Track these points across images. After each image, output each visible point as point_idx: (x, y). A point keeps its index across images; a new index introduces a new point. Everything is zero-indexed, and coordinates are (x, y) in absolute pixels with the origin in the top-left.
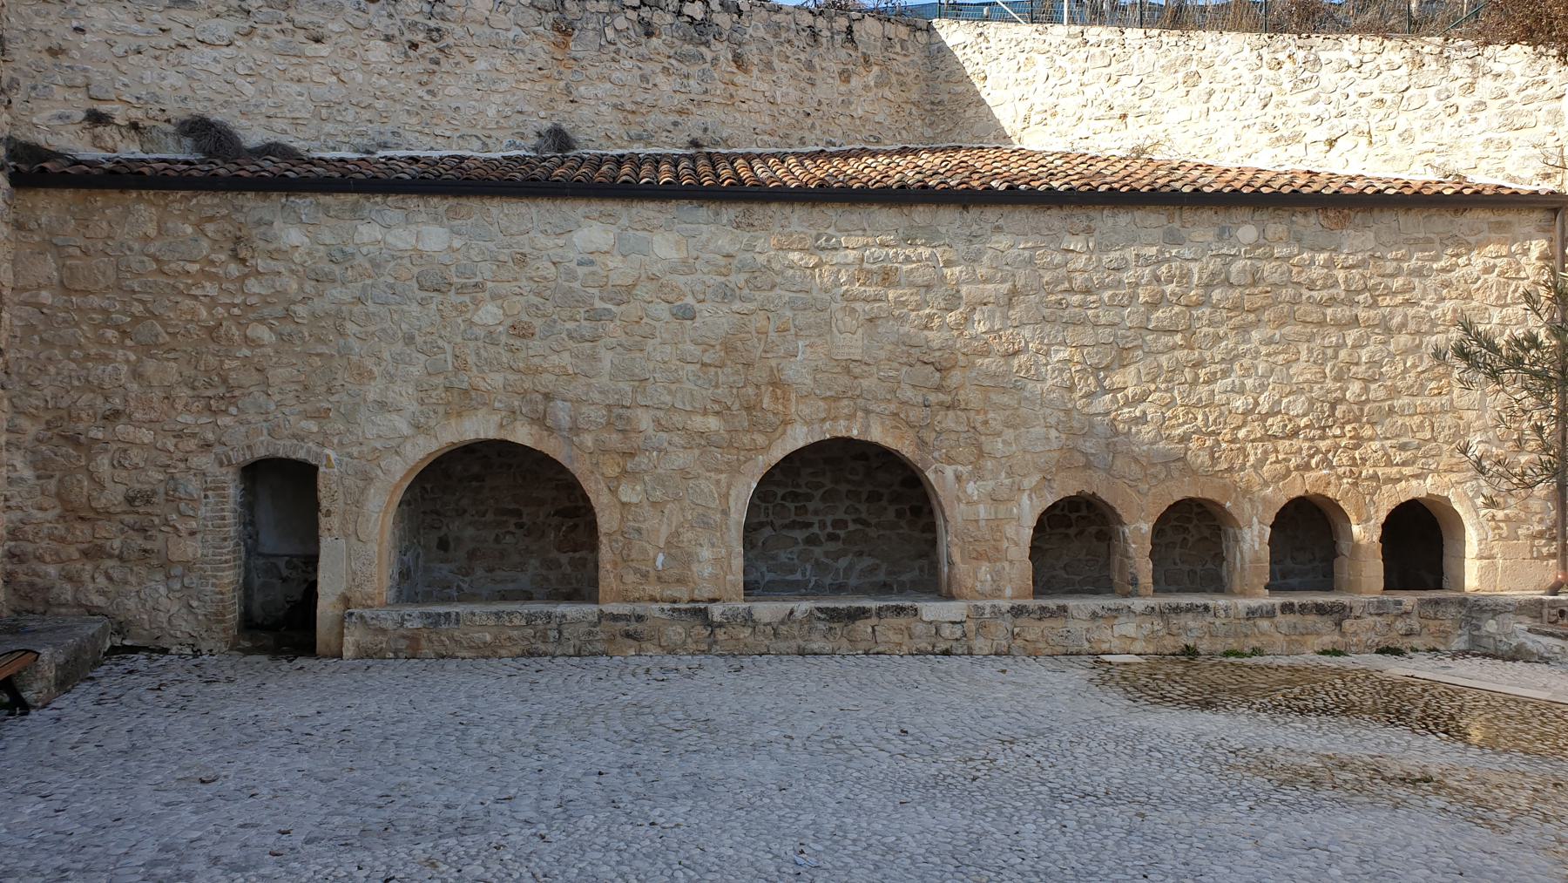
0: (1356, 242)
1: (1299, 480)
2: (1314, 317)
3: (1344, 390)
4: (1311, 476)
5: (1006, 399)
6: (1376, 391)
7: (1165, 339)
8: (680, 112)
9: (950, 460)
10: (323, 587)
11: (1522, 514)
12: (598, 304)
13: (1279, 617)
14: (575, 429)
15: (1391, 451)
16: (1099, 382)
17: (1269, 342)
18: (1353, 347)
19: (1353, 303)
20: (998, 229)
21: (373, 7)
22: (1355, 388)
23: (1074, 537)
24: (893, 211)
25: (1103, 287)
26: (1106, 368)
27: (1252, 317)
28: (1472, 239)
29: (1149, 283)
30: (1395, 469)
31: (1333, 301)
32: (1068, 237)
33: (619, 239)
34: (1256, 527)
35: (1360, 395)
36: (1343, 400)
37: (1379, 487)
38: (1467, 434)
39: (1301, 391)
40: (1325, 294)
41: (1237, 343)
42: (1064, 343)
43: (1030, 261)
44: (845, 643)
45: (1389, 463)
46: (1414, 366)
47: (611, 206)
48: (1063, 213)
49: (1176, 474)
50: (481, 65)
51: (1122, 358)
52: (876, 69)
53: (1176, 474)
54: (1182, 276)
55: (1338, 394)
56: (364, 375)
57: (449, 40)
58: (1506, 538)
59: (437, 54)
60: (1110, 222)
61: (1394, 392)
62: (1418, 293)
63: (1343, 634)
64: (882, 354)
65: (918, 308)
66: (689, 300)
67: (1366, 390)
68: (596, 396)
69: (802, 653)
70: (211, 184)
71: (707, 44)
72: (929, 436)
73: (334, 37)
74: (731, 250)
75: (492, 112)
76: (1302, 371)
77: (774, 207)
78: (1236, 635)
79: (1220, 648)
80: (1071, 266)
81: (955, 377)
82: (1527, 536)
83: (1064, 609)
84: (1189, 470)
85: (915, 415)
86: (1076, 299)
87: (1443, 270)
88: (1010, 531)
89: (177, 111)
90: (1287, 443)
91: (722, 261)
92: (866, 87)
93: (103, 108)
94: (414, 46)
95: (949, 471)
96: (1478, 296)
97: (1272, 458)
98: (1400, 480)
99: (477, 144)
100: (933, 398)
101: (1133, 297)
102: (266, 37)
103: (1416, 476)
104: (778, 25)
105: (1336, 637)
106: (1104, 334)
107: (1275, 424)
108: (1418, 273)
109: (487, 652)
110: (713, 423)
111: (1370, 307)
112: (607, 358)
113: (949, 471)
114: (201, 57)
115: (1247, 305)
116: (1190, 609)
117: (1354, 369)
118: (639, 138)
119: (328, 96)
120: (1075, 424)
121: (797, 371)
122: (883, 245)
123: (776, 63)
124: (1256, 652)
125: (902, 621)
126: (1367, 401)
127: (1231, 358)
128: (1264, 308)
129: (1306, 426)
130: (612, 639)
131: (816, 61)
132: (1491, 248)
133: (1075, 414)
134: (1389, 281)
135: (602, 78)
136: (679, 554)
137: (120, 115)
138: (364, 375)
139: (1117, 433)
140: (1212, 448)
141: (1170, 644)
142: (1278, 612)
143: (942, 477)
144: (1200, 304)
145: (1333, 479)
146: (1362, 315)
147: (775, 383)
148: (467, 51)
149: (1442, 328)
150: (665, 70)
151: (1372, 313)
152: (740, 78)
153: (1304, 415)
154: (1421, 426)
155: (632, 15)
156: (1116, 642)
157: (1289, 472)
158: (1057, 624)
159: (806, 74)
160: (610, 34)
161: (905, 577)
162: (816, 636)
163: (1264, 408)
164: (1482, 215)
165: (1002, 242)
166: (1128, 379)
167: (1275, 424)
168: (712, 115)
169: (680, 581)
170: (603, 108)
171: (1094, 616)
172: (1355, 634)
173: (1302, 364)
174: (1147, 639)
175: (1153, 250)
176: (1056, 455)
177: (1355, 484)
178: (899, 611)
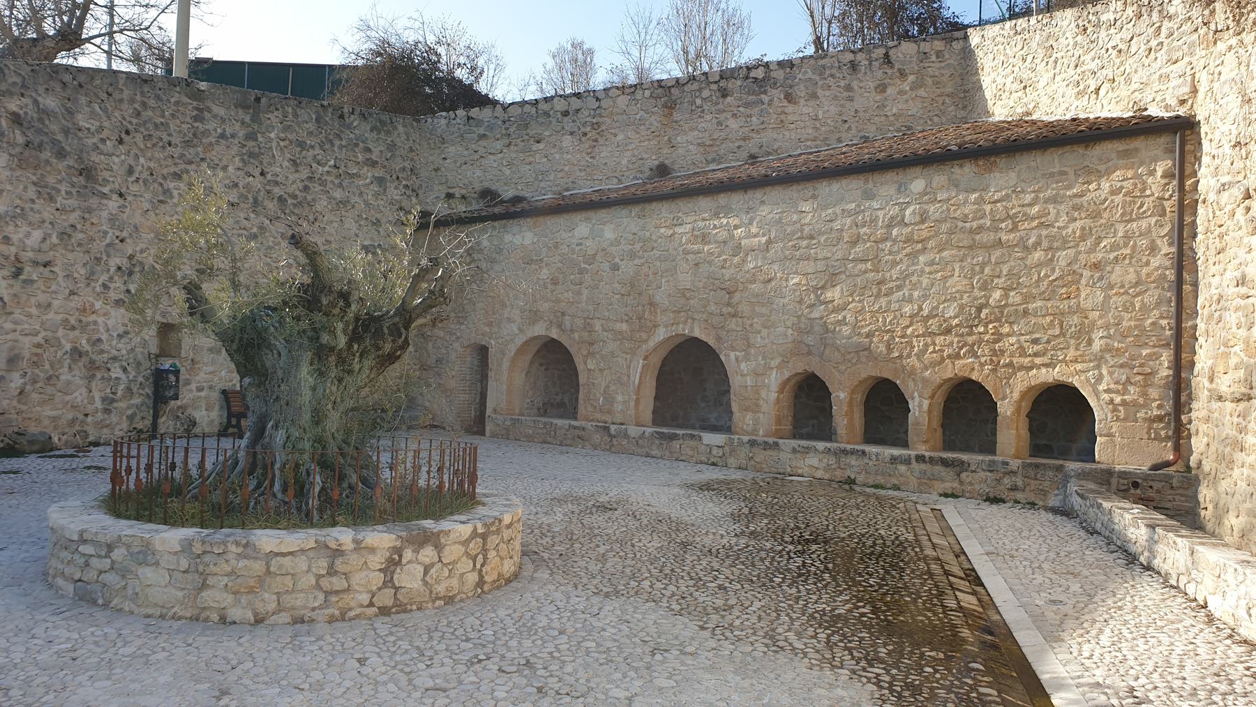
0: (1001, 182)
1: (950, 366)
2: (965, 243)
4: (959, 363)
5: (763, 310)
6: (1014, 297)
7: (862, 266)
8: (744, 139)
9: (733, 349)
10: (488, 404)
11: (1141, 401)
12: (583, 265)
13: (914, 464)
14: (572, 331)
16: (818, 297)
17: (932, 263)
18: (996, 263)
19: (997, 230)
20: (763, 202)
22: (997, 294)
23: (809, 402)
24: (709, 199)
25: (821, 233)
26: (823, 287)
27: (920, 246)
28: (1102, 168)
29: (850, 227)
30: (1028, 359)
31: (981, 229)
32: (802, 203)
33: (592, 230)
34: (917, 399)
35: (1000, 301)
36: (986, 305)
38: (1092, 331)
39: (955, 299)
40: (975, 224)
41: (908, 266)
42: (796, 273)
44: (667, 453)
45: (1023, 353)
46: (1047, 276)
47: (590, 214)
48: (800, 188)
50: (620, 137)
51: (832, 279)
52: (911, 78)
53: (864, 360)
54: (872, 221)
55: (983, 301)
56: (504, 305)
57: (604, 127)
58: (1125, 419)
60: (827, 189)
61: (1028, 298)
62: (1052, 217)
63: (961, 483)
64: (701, 285)
65: (719, 256)
66: (617, 260)
68: (580, 313)
69: (647, 456)
70: (494, 217)
71: (765, 92)
72: (723, 334)
74: (635, 231)
75: (624, 162)
76: (957, 282)
77: (654, 204)
78: (883, 474)
79: (871, 482)
80: (803, 222)
81: (737, 296)
82: (1145, 419)
83: (776, 444)
85: (715, 320)
86: (805, 243)
87: (1075, 196)
88: (763, 394)
89: (478, 187)
91: (631, 237)
92: (901, 93)
93: (451, 191)
94: (585, 134)
95: (732, 355)
96: (1106, 215)
98: (1031, 368)
99: (615, 180)
100: (725, 310)
101: (839, 239)
103: (1046, 365)
104: (824, 67)
105: (956, 485)
106: (821, 266)
107: (934, 324)
108: (1054, 200)
109: (530, 439)
110: (624, 326)
111: (1011, 231)
112: (585, 292)
113: (732, 355)
115: (916, 237)
116: (853, 452)
118: (714, 160)
120: (802, 326)
121: (661, 297)
122: (704, 220)
123: (820, 92)
124: (896, 488)
125: (693, 443)
126: (1006, 305)
127: (905, 276)
128: (929, 238)
129: (957, 325)
130: (573, 439)
131: (855, 84)
132: (1118, 173)
133: (803, 319)
134: (1027, 209)
135: (692, 129)
136: (610, 399)
137: (458, 192)
138: (504, 305)
139: (827, 331)
140: (888, 341)
141: (839, 474)
142: (913, 461)
143: (729, 358)
145: (976, 366)
146: (1004, 238)
147: (652, 304)
150: (734, 116)
151: (1012, 236)
152: (790, 109)
153: (955, 317)
154: (1051, 324)
155: (714, 87)
156: (806, 469)
157: (943, 360)
158: (773, 453)
159: (846, 94)
160: (698, 102)
161: (804, 431)
162: (654, 447)
163: (925, 313)
164: (1110, 146)
165: (764, 211)
166: (834, 294)
167: (934, 324)
168: (767, 137)
169: (609, 412)
170: (691, 147)
171: (794, 451)
172: (970, 483)
173: (956, 278)
174: (826, 470)
177: (994, 370)
178: (692, 436)
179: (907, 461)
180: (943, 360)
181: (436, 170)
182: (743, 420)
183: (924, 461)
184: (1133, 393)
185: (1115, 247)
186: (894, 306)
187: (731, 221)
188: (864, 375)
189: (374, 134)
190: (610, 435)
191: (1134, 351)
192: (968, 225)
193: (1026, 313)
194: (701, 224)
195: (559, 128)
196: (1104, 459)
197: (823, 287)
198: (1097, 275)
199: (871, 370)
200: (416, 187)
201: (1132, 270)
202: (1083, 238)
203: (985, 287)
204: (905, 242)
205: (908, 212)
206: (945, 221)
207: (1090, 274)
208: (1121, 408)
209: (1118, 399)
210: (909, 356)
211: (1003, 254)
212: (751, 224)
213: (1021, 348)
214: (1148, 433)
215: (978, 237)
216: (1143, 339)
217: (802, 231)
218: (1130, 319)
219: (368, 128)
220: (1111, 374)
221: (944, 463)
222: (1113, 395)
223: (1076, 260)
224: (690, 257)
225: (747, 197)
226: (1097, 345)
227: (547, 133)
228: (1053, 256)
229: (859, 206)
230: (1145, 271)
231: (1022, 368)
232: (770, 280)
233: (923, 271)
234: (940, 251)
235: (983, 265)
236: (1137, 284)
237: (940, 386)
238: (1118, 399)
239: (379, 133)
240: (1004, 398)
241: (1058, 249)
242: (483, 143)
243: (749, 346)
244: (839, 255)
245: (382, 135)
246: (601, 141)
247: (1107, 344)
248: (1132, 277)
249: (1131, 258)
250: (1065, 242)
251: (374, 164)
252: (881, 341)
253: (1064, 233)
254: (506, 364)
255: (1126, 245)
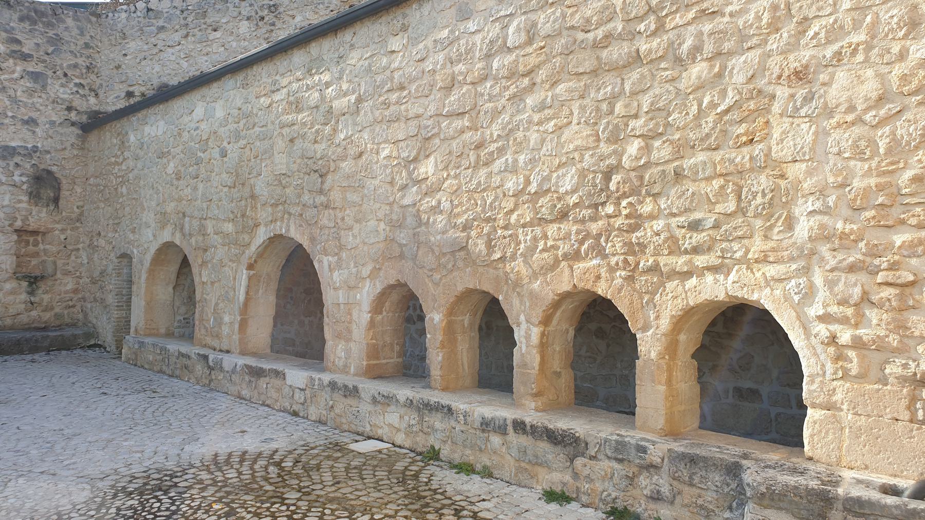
1: (567, 271)
2: (587, 66)
3: (619, 154)
4: (580, 266)
6: (661, 151)
7: (458, 123)
9: (325, 252)
11: (894, 340)
13: (512, 436)
15: (679, 233)
16: (410, 174)
17: (542, 107)
19: (633, 35)
21: (243, 3)
22: (633, 147)
25: (412, 80)
26: (415, 160)
27: (526, 81)
29: (444, 66)
35: (638, 159)
37: (663, 284)
40: (600, 33)
41: (512, 116)
43: (369, 70)
45: (674, 248)
46: (713, 105)
47: (204, 91)
49: (460, 264)
53: (460, 264)
55: (612, 161)
58: (861, 377)
59: (274, 20)
61: (681, 149)
63: (576, 476)
67: (648, 149)
73: (224, 25)
76: (576, 135)
78: (472, 447)
80: (392, 66)
82: (903, 380)
84: (471, 260)
86: (394, 97)
90: (555, 226)
93: (131, 89)
94: (262, 18)
97: (541, 245)
98: (688, 275)
102: (194, 36)
105: (568, 478)
111: (654, 34)
114: (169, 55)
117: (632, 123)
119: (219, 59)
120: (395, 217)
121: (261, 188)
125: (277, 382)
128: (538, 67)
129: (576, 205)
139: (420, 223)
140: (489, 234)
142: (510, 429)
144: (485, 78)
145: (603, 272)
146: (644, 48)
147: (253, 197)
148: (290, 13)
149: (755, 41)
153: (574, 191)
156: (386, 429)
157: (557, 262)
163: (533, 188)
165: (354, 58)
166: (427, 168)
173: (574, 127)
175: (445, 33)
176: (381, 245)
177: (630, 279)
179: (501, 429)
180: (557, 262)
181: (118, 67)
182: (336, 350)
183: (524, 431)
184: (875, 324)
185: (835, 32)
186: (496, 180)
187: (322, 77)
188: (460, 288)
189: (27, 25)
190: (209, 367)
191: (876, 237)
192: (590, 36)
193: (678, 175)
194: (295, 86)
195: (235, 14)
196: (818, 453)
197: (415, 160)
198: (801, 93)
199: (465, 281)
200: (95, 87)
201: (870, 73)
202: (774, 27)
203: (615, 138)
204: (508, 78)
205: (511, 30)
206: (560, 34)
207: (787, 91)
208: (852, 354)
209: (845, 337)
210: (513, 257)
211: (643, 77)
212: (340, 78)
213: (673, 239)
214: (911, 407)
215: (604, 54)
216: (896, 212)
217: (392, 79)
218: (868, 173)
219: (16, 16)
220: (830, 284)
221: (554, 437)
222: (835, 327)
223: (763, 68)
224: (286, 131)
225: (337, 41)
226: (803, 229)
227: (224, 20)
228: (723, 68)
229: (452, 32)
230: (898, 70)
231: (674, 274)
232: (361, 154)
233: (530, 122)
234: (554, 84)
235: (612, 99)
236: (881, 100)
237: (556, 305)
238: (845, 337)
239: (34, 23)
240: (645, 328)
241: (730, 54)
242: (162, 36)
243: (341, 248)
244: (432, 110)
245: (40, 27)
246: (279, 24)
247: (822, 227)
248: (870, 88)
249: (869, 47)
250: (743, 38)
251: (25, 57)
252: (479, 236)
253: (741, 23)
254: (144, 276)
255: (857, 25)
